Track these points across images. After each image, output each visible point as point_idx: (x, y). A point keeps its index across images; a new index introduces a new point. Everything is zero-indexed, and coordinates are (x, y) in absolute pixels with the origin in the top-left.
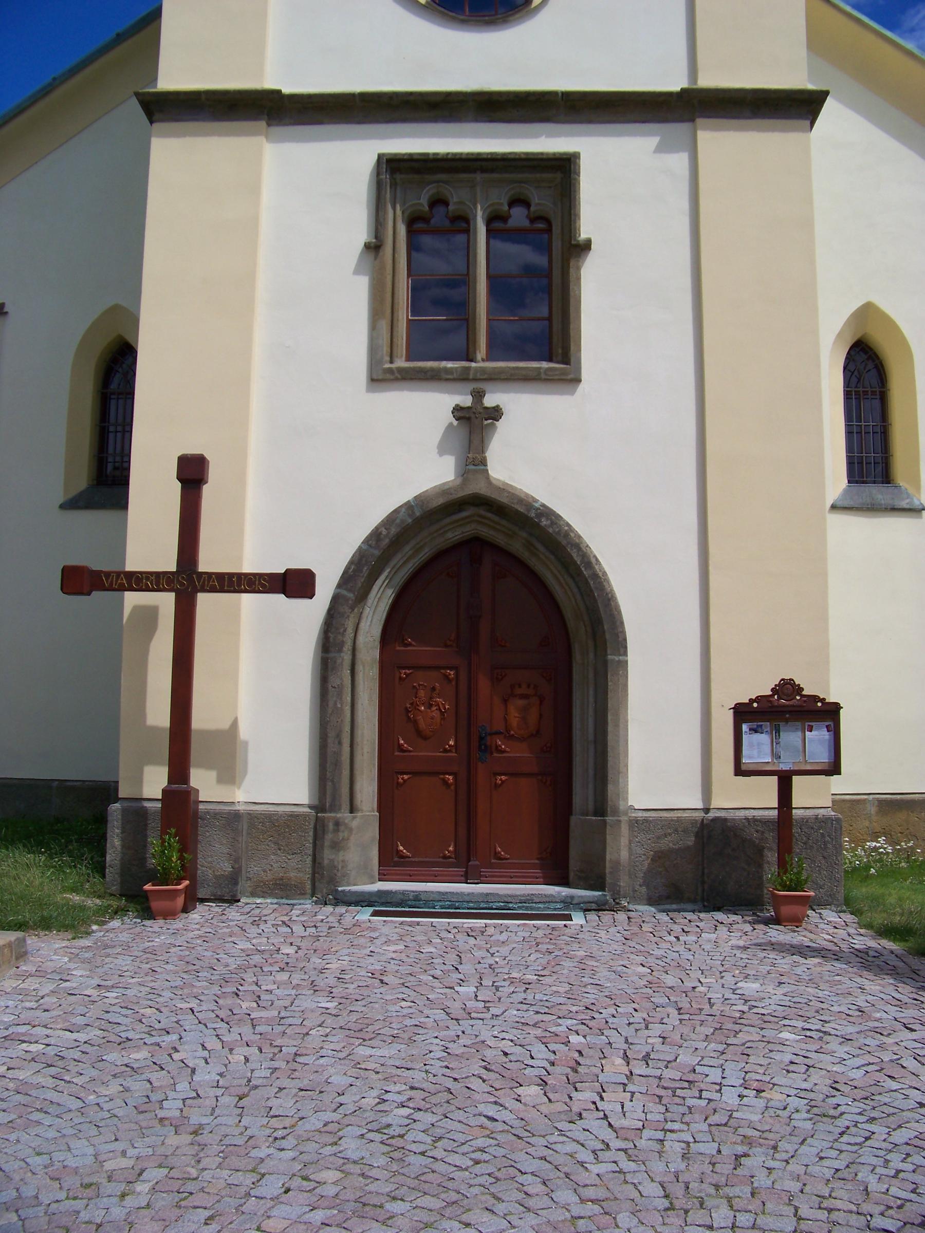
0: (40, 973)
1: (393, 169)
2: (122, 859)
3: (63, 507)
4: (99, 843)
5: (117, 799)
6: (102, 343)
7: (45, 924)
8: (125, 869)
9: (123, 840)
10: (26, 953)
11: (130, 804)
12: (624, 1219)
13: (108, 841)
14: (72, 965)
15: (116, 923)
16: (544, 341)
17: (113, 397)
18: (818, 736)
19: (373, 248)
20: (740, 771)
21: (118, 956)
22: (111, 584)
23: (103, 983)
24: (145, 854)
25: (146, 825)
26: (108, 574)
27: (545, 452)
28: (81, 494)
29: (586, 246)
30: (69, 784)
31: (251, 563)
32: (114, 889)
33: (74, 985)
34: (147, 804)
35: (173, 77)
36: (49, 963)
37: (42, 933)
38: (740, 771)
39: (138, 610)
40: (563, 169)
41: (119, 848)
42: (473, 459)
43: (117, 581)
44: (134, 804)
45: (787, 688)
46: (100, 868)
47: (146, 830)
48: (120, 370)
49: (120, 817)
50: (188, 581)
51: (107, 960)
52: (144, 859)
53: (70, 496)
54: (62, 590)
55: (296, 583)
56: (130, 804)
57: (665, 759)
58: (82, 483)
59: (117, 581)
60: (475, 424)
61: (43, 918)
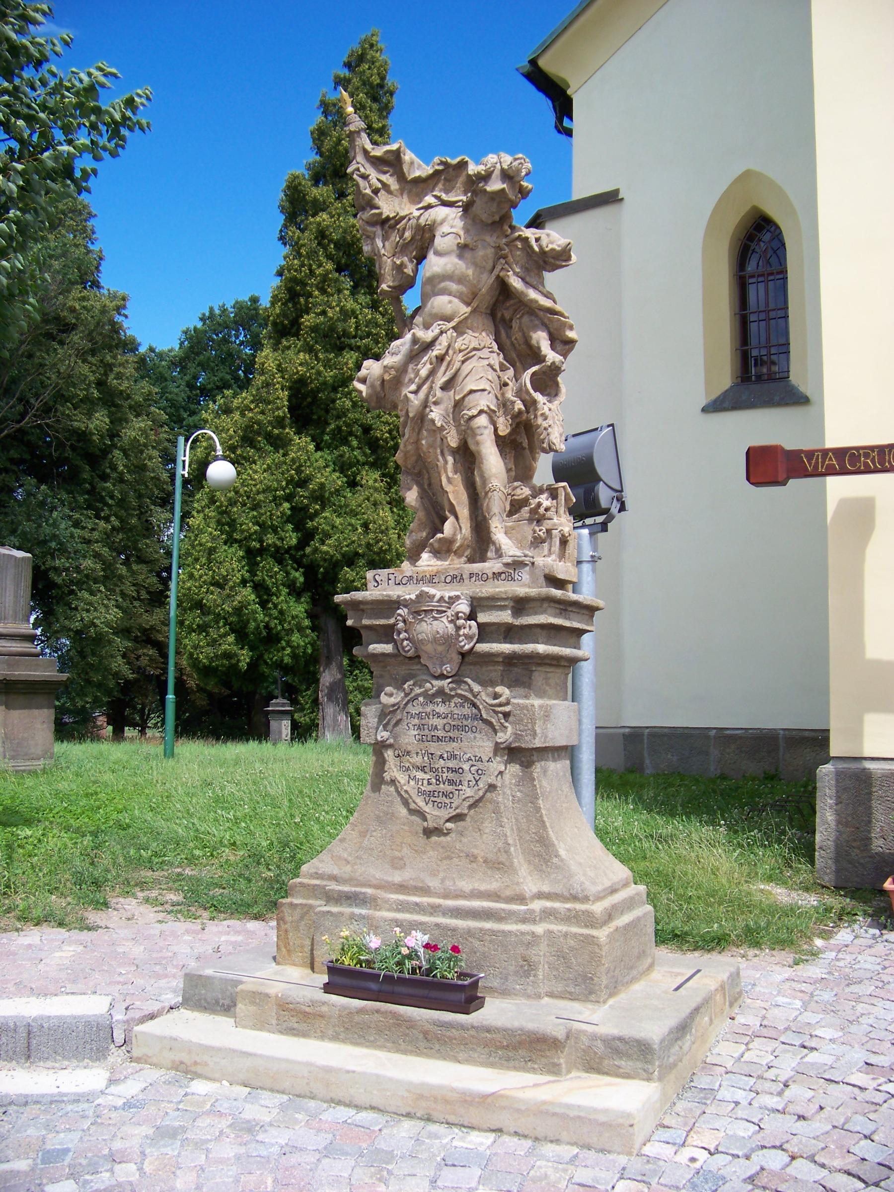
0: (765, 1031)
2: (837, 838)
3: (705, 410)
4: (803, 813)
5: (827, 760)
7: (752, 938)
8: (841, 854)
9: (838, 813)
10: (740, 993)
11: (845, 765)
13: (818, 815)
14: (810, 1017)
15: (844, 935)
17: (751, 281)
21: (875, 1001)
22: (816, 467)
23: (873, 1059)
24: (869, 832)
25: (870, 793)
26: (810, 454)
28: (725, 394)
30: (728, 732)
32: (828, 879)
33: (829, 1060)
34: (869, 765)
36: (776, 1011)
37: (751, 952)
39: (846, 504)
41: (833, 824)
43: (823, 463)
44: (853, 766)
46: (808, 851)
47: (870, 800)
48: (757, 249)
49: (833, 782)
51: (861, 1008)
52: (867, 841)
53: (713, 397)
54: (748, 479)
56: (845, 765)
58: (725, 380)
59: (823, 463)
61: (748, 931)
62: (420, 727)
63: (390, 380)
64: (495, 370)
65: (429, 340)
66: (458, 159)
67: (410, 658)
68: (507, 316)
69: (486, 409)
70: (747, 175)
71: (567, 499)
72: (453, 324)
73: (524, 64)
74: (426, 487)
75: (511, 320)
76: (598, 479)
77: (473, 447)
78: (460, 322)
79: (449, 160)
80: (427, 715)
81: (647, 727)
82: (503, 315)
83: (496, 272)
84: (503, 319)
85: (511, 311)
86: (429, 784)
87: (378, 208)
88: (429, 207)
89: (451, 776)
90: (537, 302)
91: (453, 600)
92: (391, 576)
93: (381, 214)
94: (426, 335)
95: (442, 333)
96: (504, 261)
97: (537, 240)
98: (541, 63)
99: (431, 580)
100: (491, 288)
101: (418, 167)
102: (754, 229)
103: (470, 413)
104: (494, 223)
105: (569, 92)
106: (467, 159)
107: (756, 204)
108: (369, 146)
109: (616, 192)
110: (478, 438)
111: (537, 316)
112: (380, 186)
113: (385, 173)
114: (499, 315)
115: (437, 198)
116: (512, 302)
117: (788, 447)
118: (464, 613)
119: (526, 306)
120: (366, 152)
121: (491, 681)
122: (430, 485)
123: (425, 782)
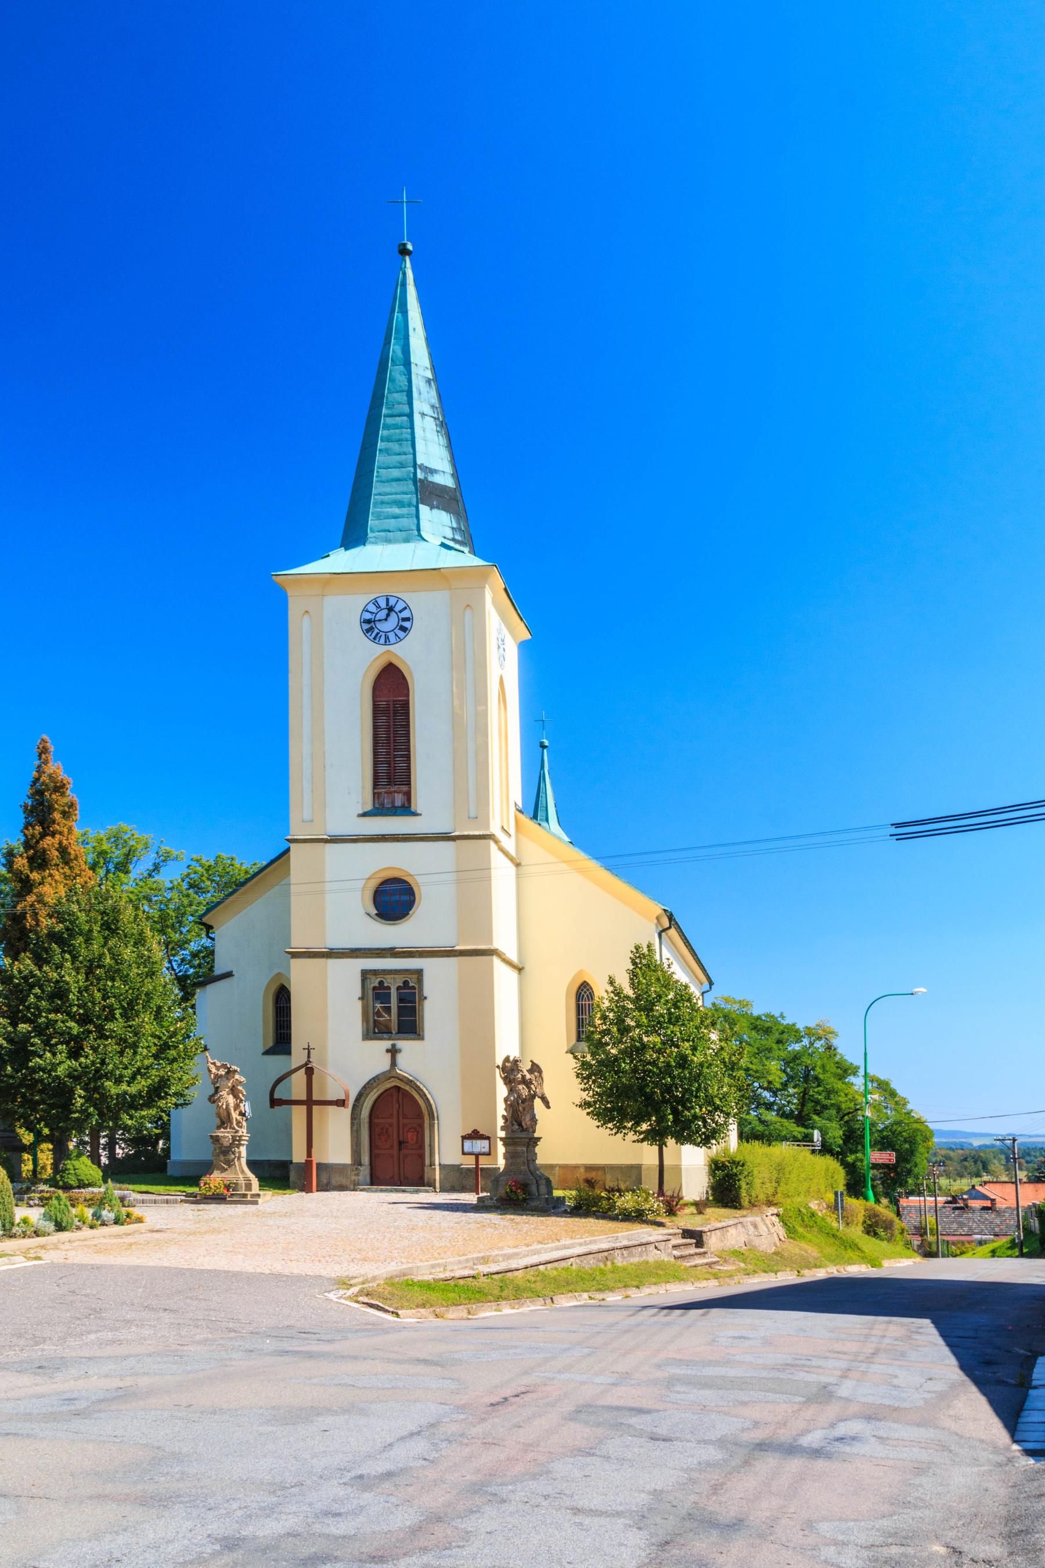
1: (365, 974)
3: (264, 1054)
6: (274, 987)
12: (995, 1564)
16: (410, 1025)
18: (486, 1143)
19: (362, 998)
20: (464, 1153)
27: (415, 1060)
29: (426, 998)
31: (330, 1098)
35: (299, 941)
38: (464, 1153)
40: (419, 973)
42: (394, 1063)
45: (476, 1132)
50: (309, 1103)
55: (341, 1103)
57: (447, 1149)
58: (270, 1044)
60: (393, 1052)
101: (218, 1064)
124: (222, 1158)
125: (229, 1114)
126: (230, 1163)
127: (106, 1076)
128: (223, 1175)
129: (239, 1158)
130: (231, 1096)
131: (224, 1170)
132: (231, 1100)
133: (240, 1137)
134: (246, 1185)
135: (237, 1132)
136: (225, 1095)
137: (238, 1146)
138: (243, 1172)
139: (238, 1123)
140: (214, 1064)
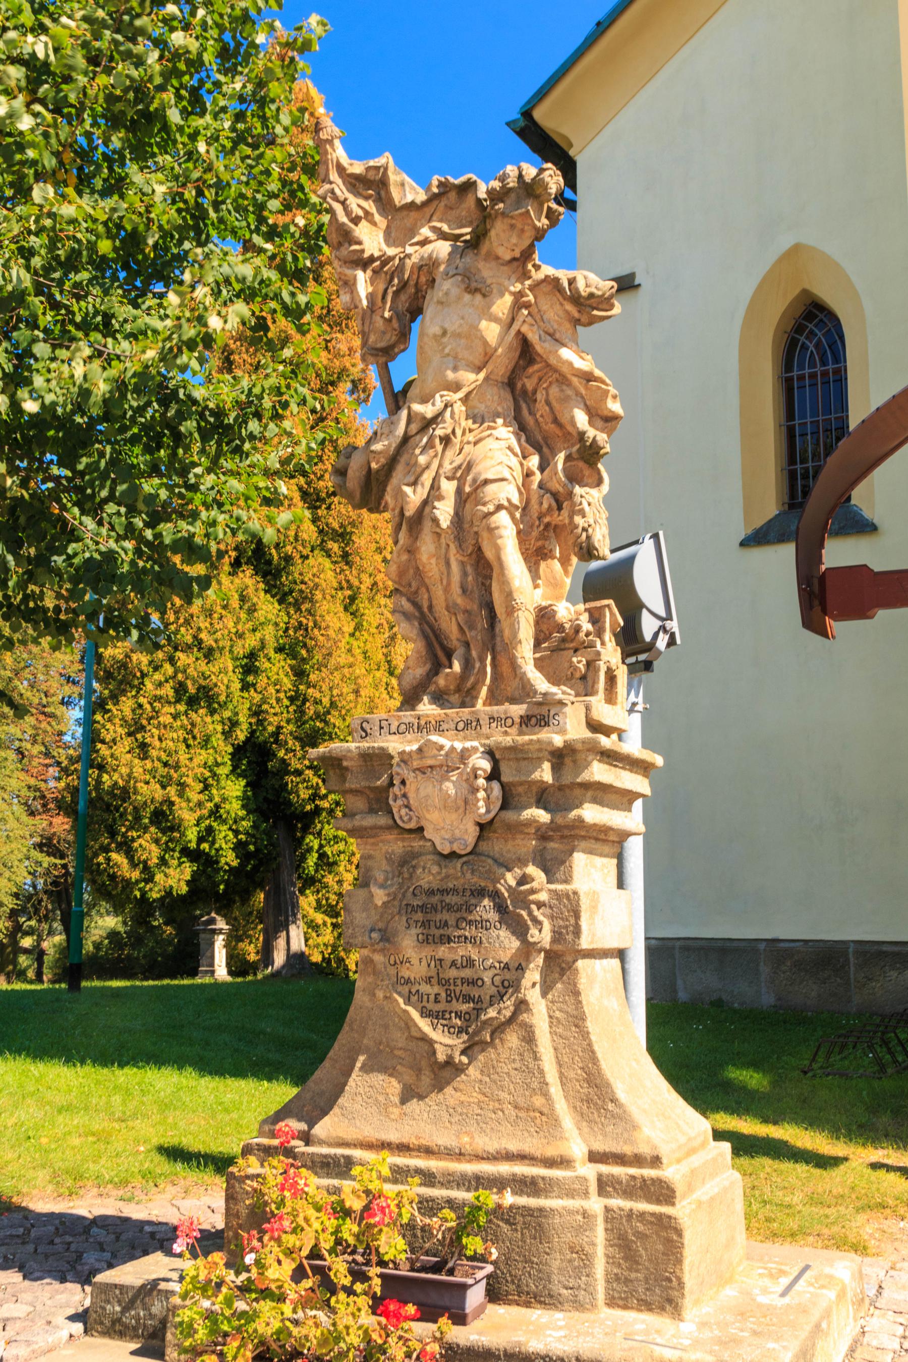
3: (745, 543)
53: (759, 522)
62: (425, 924)
63: (378, 471)
64: (516, 455)
65: (429, 415)
66: (463, 179)
67: (410, 831)
68: (530, 385)
69: (506, 504)
70: (796, 250)
71: (614, 621)
72: (460, 394)
73: (515, 115)
74: (426, 610)
75: (535, 392)
76: (641, 606)
77: (489, 554)
78: (470, 393)
79: (451, 180)
80: (434, 909)
81: (679, 939)
82: (524, 385)
83: (515, 327)
84: (524, 392)
85: (535, 380)
86: (436, 1001)
87: (360, 243)
88: (424, 243)
89: (466, 989)
90: (570, 364)
91: (464, 756)
92: (384, 723)
93: (363, 251)
94: (428, 410)
95: (446, 406)
96: (526, 312)
97: (572, 282)
98: (537, 114)
99: (438, 728)
100: (510, 348)
101: (408, 190)
102: (804, 319)
103: (485, 509)
104: (514, 259)
105: (571, 153)
106: (474, 178)
107: (808, 287)
108: (345, 160)
109: (632, 276)
110: (499, 541)
111: (569, 384)
112: (361, 213)
113: (367, 198)
114: (519, 385)
115: (434, 229)
116: (536, 367)
117: (877, 568)
118: (484, 771)
119: (556, 371)
120: (340, 169)
121: (519, 860)
122: (430, 607)
123: (432, 998)
124: (414, 956)
125: (483, 568)
126: (478, 1009)
127: (288, 773)
128: (423, 1122)
129: (561, 962)
130: (504, 434)
131: (430, 1075)
132: (500, 458)
133: (562, 757)
134: (624, 1239)
135: (541, 715)
136: (457, 419)
137: (556, 847)
138: (595, 1095)
139: (554, 638)
140: (373, 185)
